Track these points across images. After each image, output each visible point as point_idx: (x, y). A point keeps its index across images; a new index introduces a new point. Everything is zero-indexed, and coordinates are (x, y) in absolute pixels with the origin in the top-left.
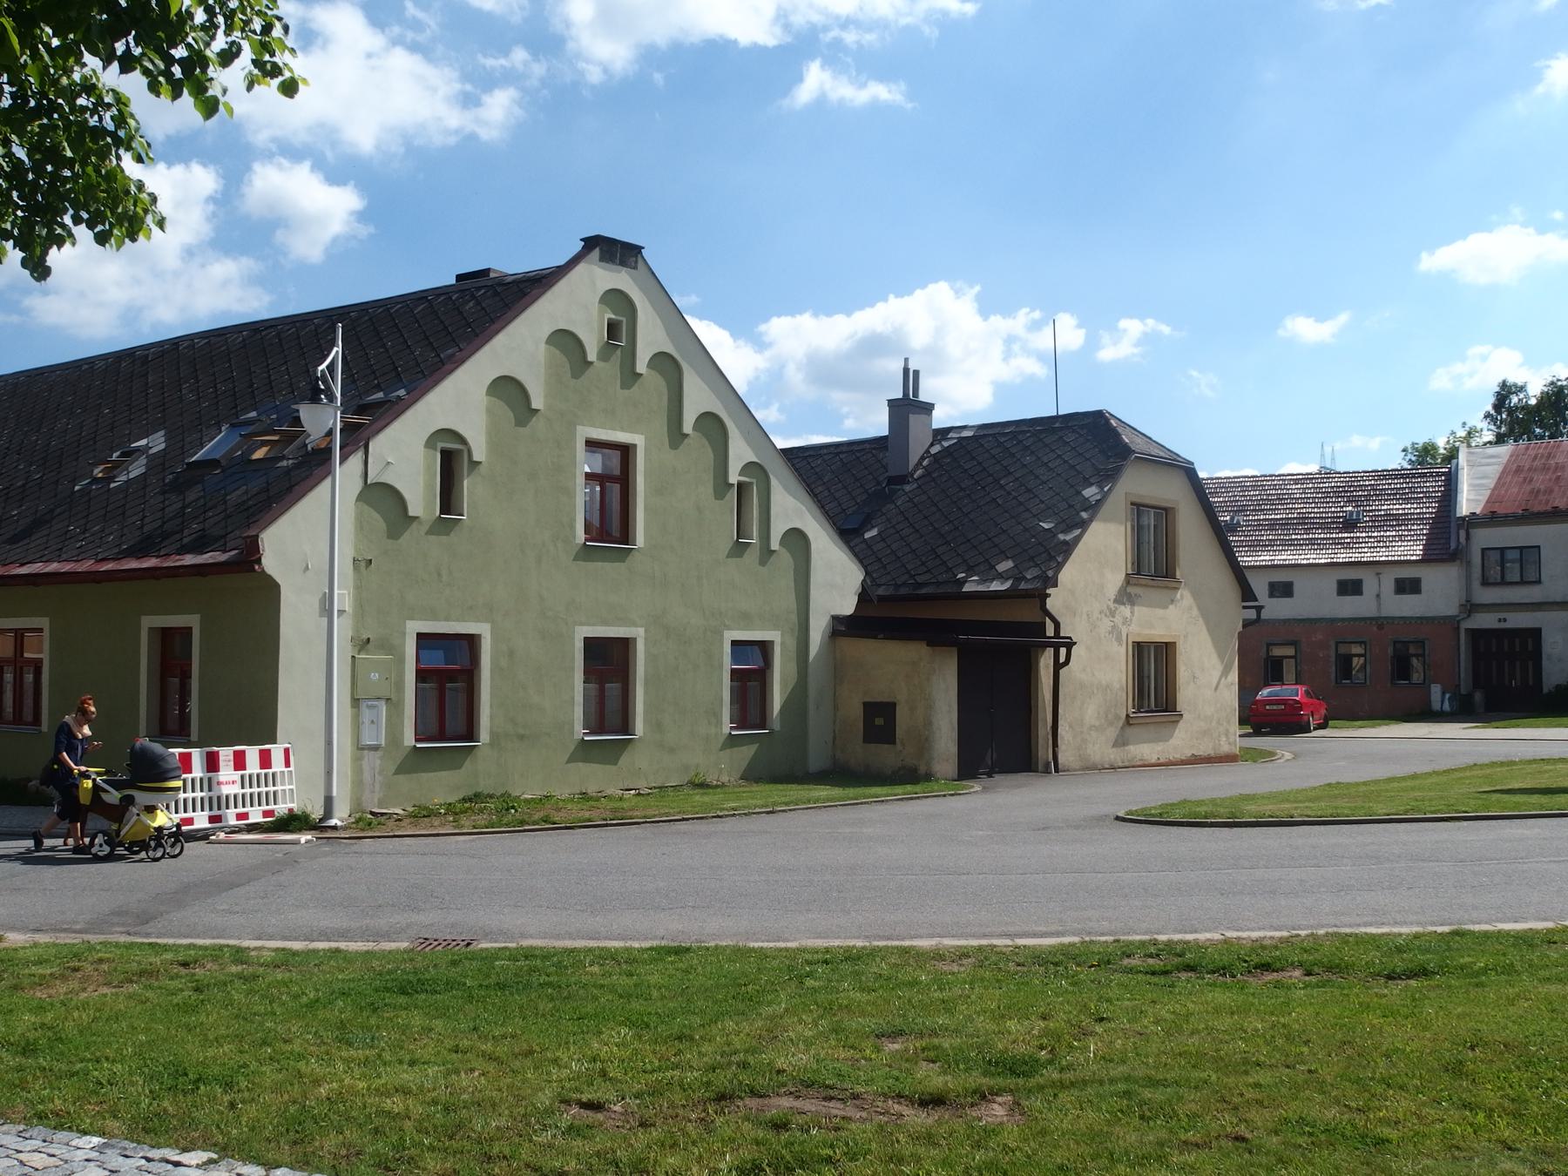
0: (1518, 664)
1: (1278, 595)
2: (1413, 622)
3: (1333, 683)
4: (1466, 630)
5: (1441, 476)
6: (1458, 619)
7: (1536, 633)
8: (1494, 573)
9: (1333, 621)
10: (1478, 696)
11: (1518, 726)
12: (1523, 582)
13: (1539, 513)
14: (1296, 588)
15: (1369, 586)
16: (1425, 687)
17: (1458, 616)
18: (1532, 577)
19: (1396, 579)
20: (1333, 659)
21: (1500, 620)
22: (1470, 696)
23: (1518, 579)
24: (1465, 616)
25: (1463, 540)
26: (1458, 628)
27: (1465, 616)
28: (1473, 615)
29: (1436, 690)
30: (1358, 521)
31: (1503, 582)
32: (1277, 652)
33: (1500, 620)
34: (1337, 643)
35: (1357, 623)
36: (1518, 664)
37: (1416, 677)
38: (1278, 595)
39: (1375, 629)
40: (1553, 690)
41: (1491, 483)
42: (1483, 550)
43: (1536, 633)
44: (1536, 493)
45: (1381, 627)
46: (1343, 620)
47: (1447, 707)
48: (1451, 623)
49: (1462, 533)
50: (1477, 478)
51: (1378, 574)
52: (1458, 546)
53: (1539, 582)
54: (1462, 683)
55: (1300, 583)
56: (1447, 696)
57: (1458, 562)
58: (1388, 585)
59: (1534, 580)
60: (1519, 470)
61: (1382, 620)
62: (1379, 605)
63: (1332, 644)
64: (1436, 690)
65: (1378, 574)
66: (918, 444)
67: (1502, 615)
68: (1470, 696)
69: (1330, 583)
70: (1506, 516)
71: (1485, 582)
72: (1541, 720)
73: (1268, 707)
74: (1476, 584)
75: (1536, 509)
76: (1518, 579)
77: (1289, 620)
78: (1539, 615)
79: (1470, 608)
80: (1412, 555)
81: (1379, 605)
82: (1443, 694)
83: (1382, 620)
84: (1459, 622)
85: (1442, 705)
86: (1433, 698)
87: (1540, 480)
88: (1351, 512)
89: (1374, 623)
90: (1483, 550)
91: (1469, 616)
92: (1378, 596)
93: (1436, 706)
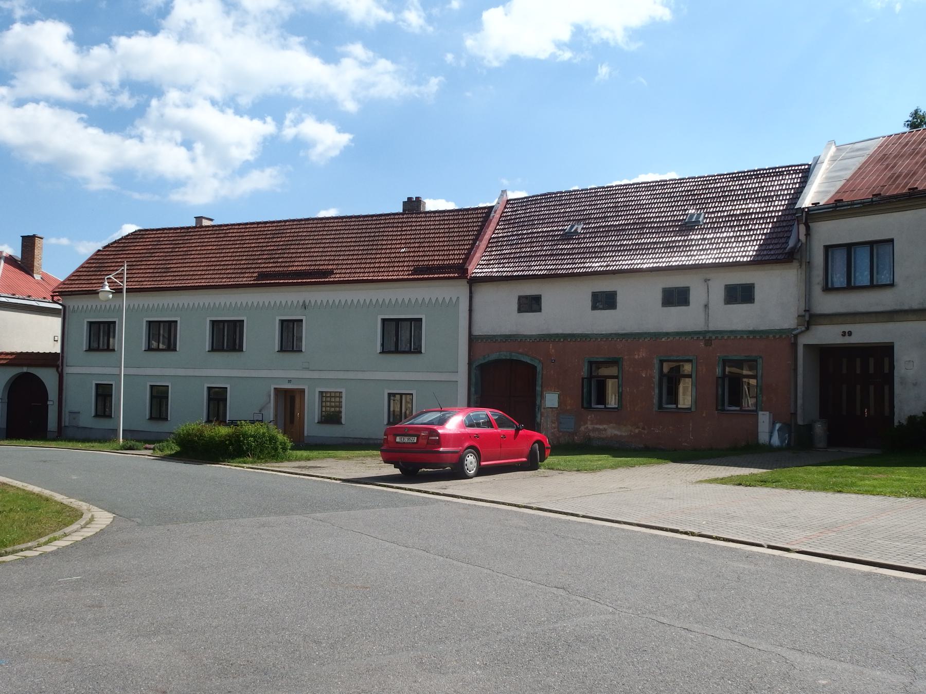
0: (872, 388)
1: (601, 307)
2: (745, 336)
3: (655, 408)
4: (806, 346)
5: (799, 173)
6: (794, 332)
7: (886, 351)
8: (839, 279)
9: (656, 336)
10: (819, 429)
11: (795, 485)
12: (873, 286)
13: (891, 197)
14: (620, 299)
15: (697, 296)
16: (754, 414)
17: (794, 329)
18: (884, 279)
19: (726, 286)
20: (656, 379)
21: (844, 334)
22: (809, 427)
23: (866, 282)
24: (803, 329)
25: (803, 238)
26: (795, 345)
27: (803, 329)
28: (813, 328)
29: (764, 419)
30: (697, 222)
31: (850, 287)
32: (604, 371)
33: (844, 334)
34: (661, 362)
35: (683, 338)
36: (872, 388)
37: (749, 402)
38: (601, 307)
39: (702, 344)
40: (905, 423)
41: (848, 174)
42: (827, 248)
43: (886, 351)
44: (895, 178)
45: (708, 342)
46: (667, 334)
47: (776, 441)
48: (788, 338)
49: (802, 228)
50: (835, 171)
51: (706, 280)
52: (796, 245)
53: (892, 285)
54: (799, 411)
55: (624, 291)
56: (778, 426)
57: (796, 264)
58: (718, 294)
59: (888, 283)
60: (884, 157)
61: (710, 335)
62: (707, 315)
63: (656, 362)
64: (764, 419)
65: (706, 280)
66: (114, 108)
67: (847, 328)
68: (809, 427)
69: (654, 291)
70: (852, 203)
71: (828, 288)
72: (815, 472)
73: (398, 439)
74: (817, 289)
75: (893, 191)
76: (866, 282)
77: (611, 334)
78: (890, 326)
79: (810, 319)
80: (744, 257)
81: (707, 315)
82: (774, 424)
83: (710, 335)
84: (796, 336)
85: (770, 439)
86: (760, 429)
87: (903, 166)
88: (692, 215)
89: (701, 338)
90: (827, 248)
91: (808, 329)
92: (706, 306)
93: (763, 438)
